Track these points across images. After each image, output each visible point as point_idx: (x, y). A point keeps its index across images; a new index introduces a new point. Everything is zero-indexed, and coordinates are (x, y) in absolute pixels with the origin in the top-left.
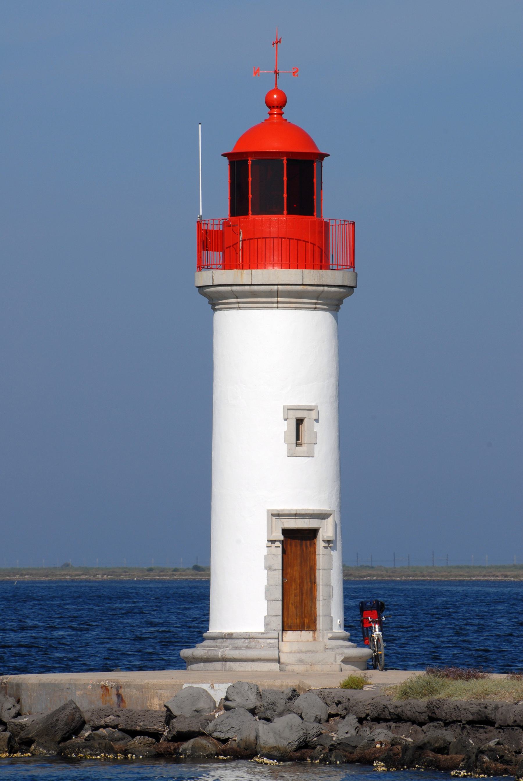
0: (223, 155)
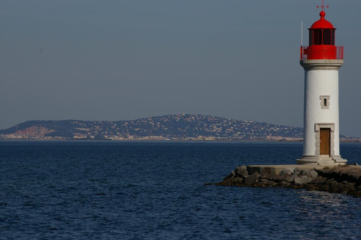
0: (308, 29)
